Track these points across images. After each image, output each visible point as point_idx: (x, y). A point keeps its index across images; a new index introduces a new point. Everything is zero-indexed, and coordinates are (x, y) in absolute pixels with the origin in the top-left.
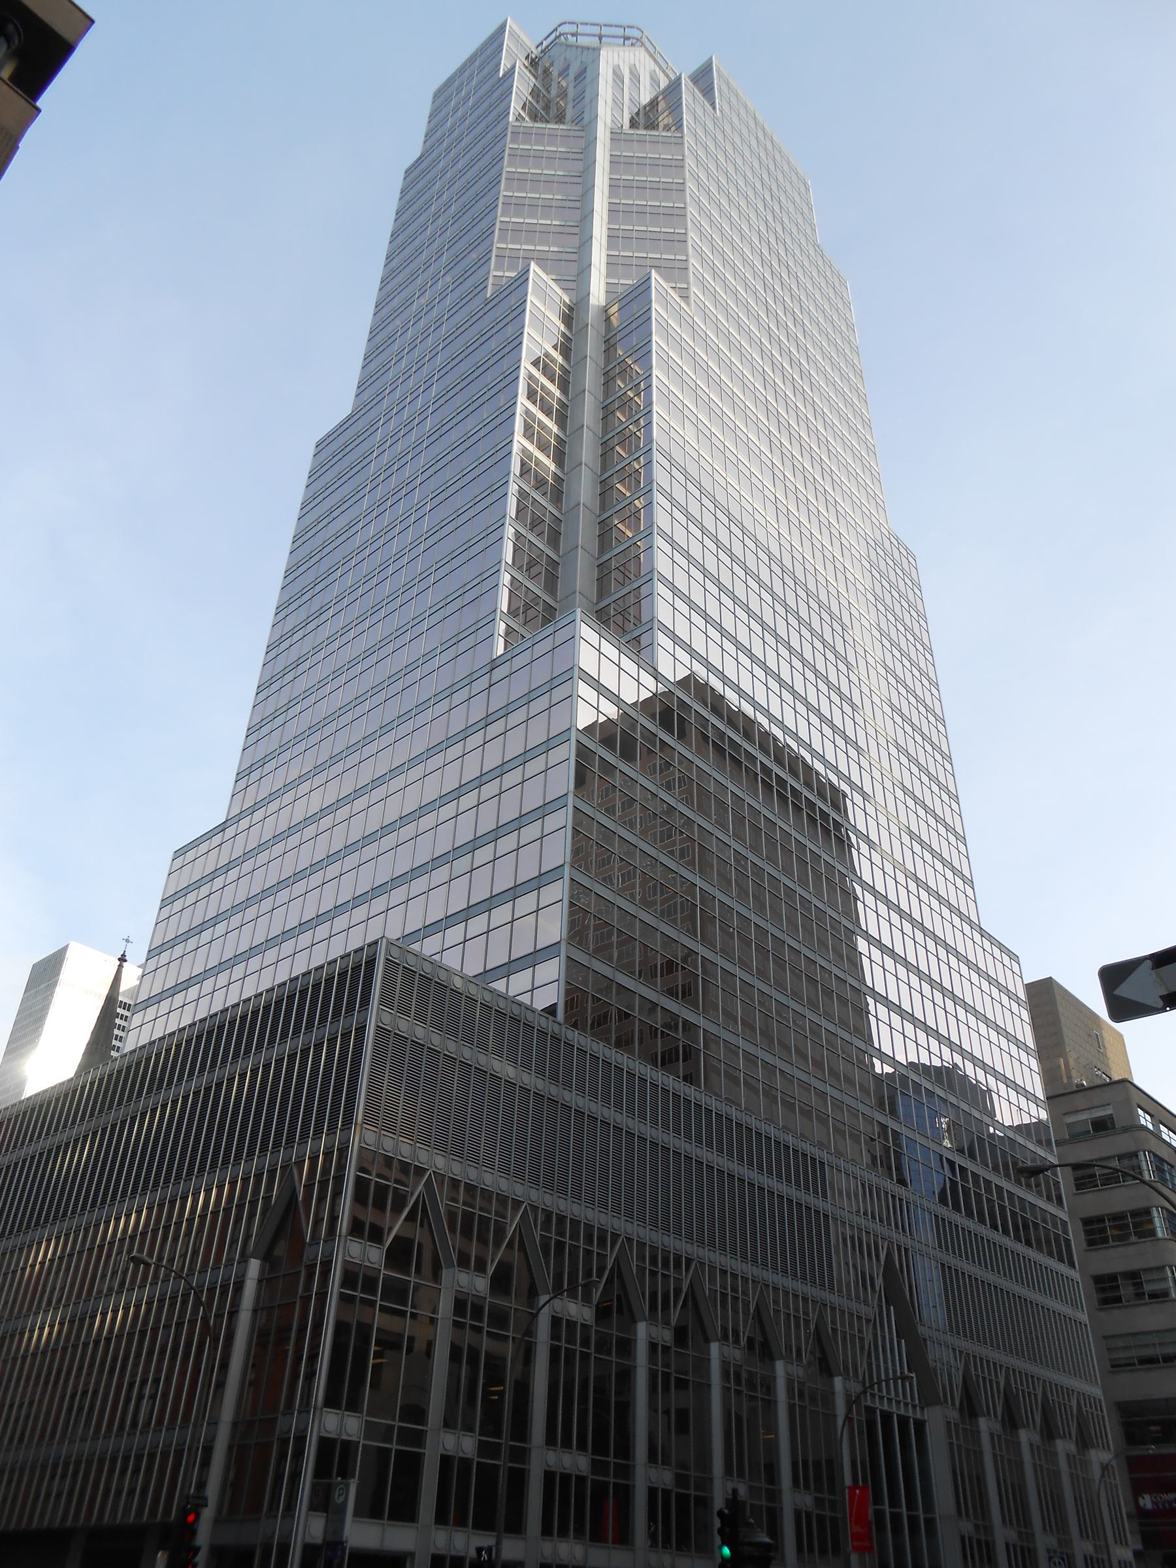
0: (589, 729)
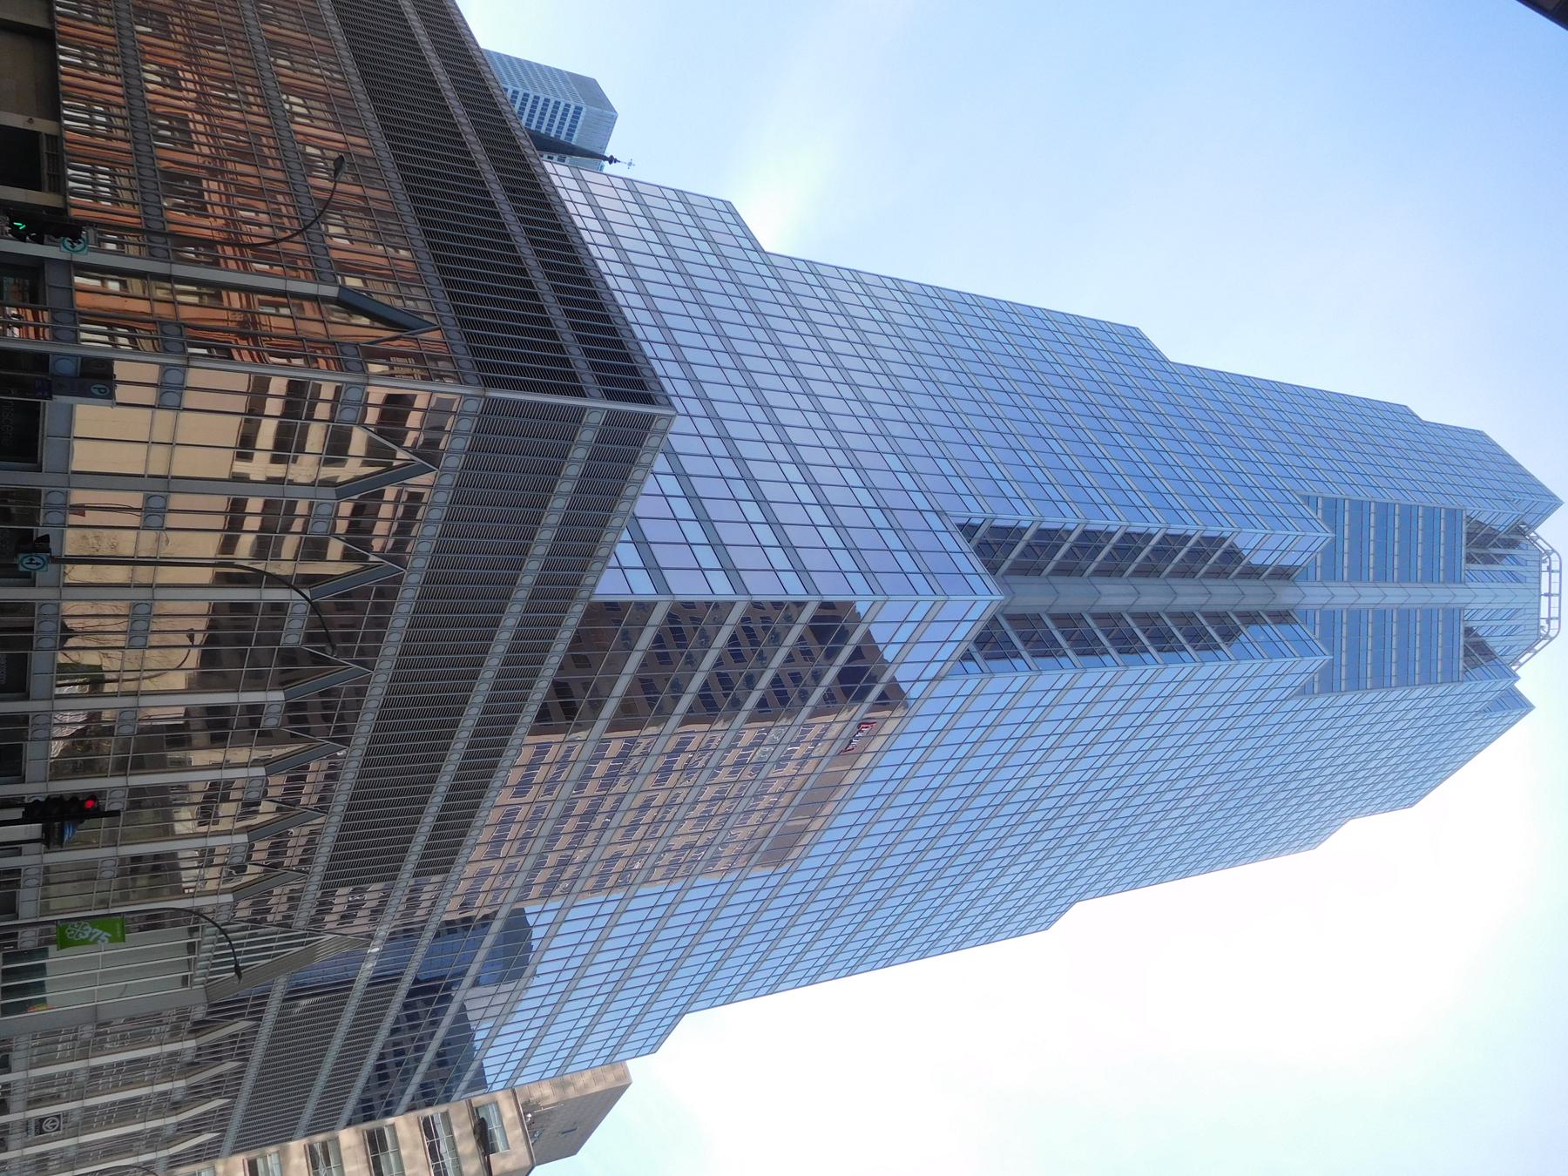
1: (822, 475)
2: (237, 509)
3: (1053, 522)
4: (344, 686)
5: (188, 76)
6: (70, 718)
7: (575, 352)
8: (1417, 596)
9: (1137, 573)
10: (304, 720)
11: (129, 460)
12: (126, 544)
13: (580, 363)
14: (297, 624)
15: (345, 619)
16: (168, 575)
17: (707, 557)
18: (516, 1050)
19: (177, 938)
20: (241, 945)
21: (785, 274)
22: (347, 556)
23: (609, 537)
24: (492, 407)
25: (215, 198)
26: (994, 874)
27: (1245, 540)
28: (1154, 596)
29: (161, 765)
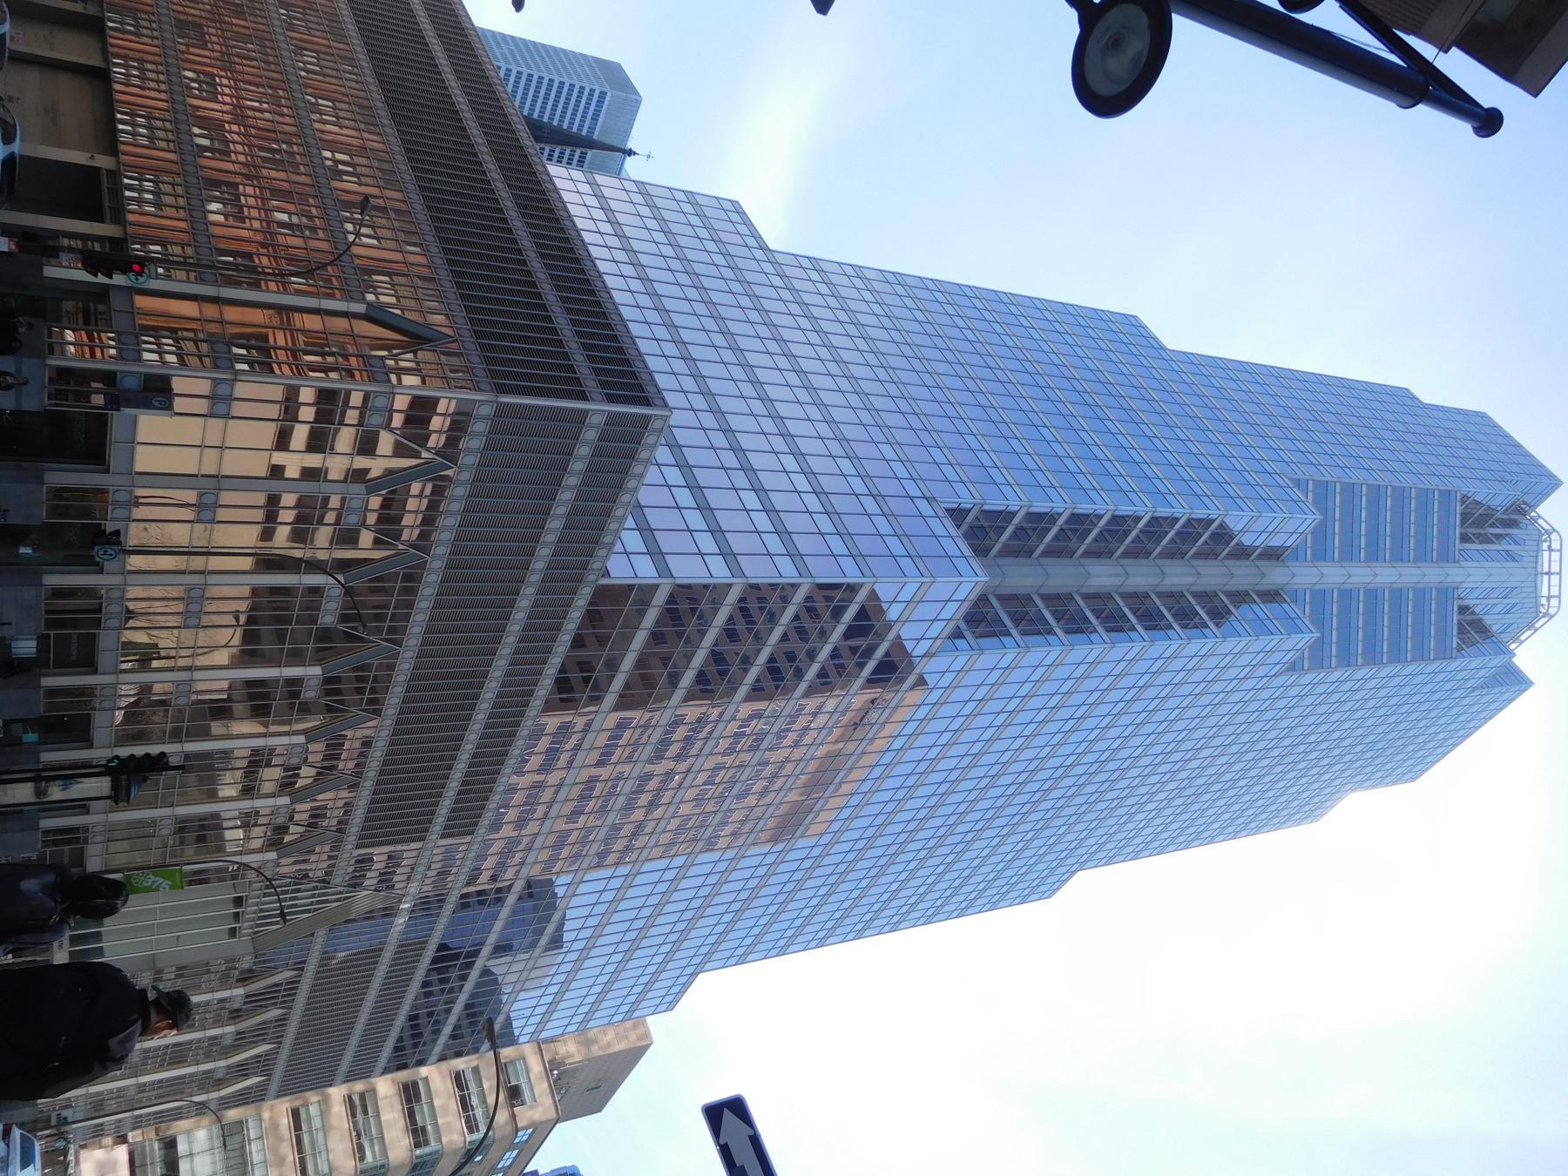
0: (873, 595)
1: (817, 464)
2: (273, 501)
3: (1040, 507)
4: (375, 662)
5: (225, 81)
6: (128, 692)
7: (579, 359)
8: (1408, 575)
9: (1126, 554)
10: (338, 692)
11: (185, 462)
12: (180, 535)
13: (584, 369)
14: (332, 606)
15: (375, 600)
16: (216, 563)
17: (707, 543)
18: (543, 1007)
19: (223, 893)
20: (286, 892)
21: (789, 271)
22: (377, 543)
23: (613, 526)
24: (502, 411)
25: (252, 201)
26: (994, 842)
27: (1235, 522)
28: (1142, 576)
29: (205, 734)
